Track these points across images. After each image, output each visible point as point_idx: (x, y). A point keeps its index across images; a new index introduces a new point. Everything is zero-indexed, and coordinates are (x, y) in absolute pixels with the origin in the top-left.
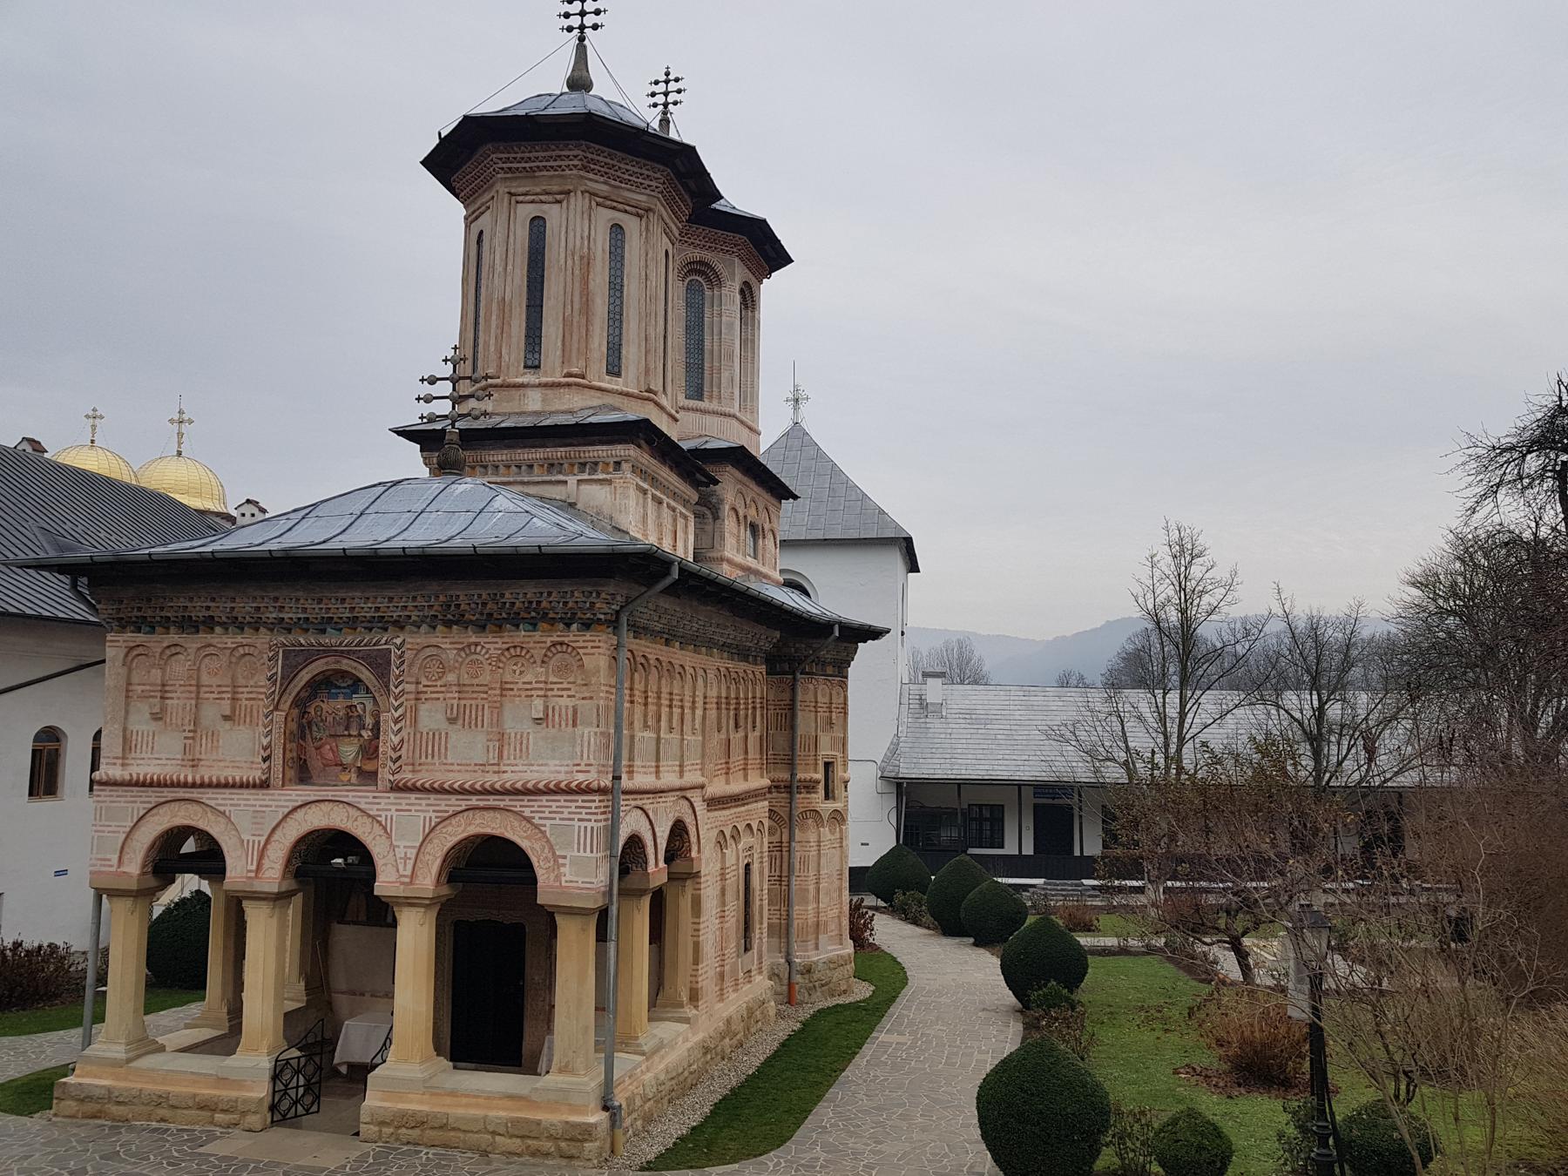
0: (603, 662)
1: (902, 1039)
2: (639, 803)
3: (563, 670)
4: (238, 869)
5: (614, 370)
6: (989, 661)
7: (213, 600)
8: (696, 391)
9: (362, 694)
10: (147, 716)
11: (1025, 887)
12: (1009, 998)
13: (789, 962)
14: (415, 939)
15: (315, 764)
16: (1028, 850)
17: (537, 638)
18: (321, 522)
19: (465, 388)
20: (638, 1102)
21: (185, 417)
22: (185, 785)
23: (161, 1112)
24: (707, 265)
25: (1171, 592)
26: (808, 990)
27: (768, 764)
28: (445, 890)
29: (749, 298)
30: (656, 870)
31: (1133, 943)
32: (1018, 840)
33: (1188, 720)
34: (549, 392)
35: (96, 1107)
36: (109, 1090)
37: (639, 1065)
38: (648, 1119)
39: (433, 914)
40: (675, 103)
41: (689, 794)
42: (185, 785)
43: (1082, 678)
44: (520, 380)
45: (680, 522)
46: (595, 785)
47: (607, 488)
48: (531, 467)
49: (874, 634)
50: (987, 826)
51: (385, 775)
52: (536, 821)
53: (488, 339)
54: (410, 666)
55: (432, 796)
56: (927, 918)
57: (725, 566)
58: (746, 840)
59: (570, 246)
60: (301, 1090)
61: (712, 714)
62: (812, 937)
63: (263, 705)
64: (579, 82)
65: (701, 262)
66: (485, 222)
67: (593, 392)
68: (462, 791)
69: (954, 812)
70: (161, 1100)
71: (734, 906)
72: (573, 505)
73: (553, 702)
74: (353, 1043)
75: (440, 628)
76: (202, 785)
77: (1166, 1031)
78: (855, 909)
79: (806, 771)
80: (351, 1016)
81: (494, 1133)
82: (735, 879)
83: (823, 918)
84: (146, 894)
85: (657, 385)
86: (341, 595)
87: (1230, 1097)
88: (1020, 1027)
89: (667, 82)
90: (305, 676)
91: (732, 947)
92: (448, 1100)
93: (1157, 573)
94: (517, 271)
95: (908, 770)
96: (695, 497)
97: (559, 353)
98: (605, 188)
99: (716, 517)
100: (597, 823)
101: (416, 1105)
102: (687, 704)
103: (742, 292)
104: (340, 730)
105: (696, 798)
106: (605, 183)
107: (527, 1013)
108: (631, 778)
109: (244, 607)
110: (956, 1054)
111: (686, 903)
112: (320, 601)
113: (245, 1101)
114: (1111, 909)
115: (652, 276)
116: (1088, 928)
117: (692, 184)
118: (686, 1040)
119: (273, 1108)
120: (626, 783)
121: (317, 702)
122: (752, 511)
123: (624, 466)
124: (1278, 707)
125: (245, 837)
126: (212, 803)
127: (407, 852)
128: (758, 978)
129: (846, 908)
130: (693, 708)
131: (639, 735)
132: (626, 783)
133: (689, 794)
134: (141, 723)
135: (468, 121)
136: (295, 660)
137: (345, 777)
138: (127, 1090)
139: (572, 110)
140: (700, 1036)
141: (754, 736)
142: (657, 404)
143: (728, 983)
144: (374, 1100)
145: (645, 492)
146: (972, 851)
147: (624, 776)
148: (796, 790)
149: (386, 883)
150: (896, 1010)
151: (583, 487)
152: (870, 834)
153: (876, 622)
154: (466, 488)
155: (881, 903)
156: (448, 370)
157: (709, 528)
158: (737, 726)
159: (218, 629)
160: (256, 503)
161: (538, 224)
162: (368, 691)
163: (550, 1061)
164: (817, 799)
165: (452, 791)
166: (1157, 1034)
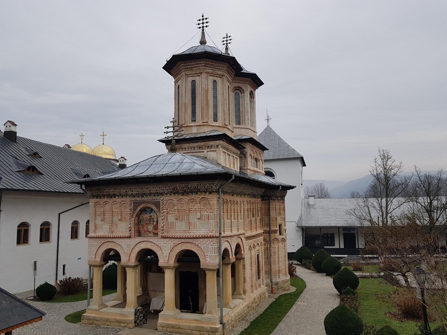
0: (215, 202)
1: (304, 304)
2: (227, 240)
3: (205, 205)
4: (124, 259)
5: (215, 120)
6: (329, 188)
7: (115, 189)
8: (238, 123)
9: (153, 213)
10: (100, 220)
11: (342, 258)
12: (336, 292)
13: (271, 281)
14: (169, 277)
15: (142, 231)
16: (342, 246)
17: (198, 197)
18: (141, 167)
19: (176, 128)
20: (230, 322)
21: (105, 134)
22: (110, 238)
23: (108, 323)
24: (240, 87)
25: (382, 170)
26: (277, 289)
27: (262, 226)
28: (177, 264)
29: (252, 95)
30: (232, 257)
31: (374, 274)
32: (339, 244)
33: (389, 207)
34: (198, 127)
35: (92, 322)
36: (95, 317)
37: (230, 311)
38: (233, 326)
39: (174, 271)
40: (229, 43)
41: (240, 236)
42: (110, 238)
43: (358, 193)
44: (190, 125)
45: (235, 159)
46: (214, 236)
47: (215, 153)
49: (292, 188)
50: (329, 240)
51: (160, 234)
52: (199, 246)
53: (182, 114)
54: (165, 205)
55: (172, 239)
56: (312, 268)
57: (248, 171)
58: (257, 248)
59: (202, 87)
60: (142, 318)
61: (246, 213)
62: (278, 274)
63: (128, 217)
64: (203, 42)
65: (238, 87)
66: (180, 83)
67: (210, 127)
68: (180, 238)
69: (319, 236)
70: (107, 320)
71: (255, 267)
72: (206, 158)
73: (203, 213)
74: (154, 305)
75: (172, 195)
76: (114, 238)
77: (383, 301)
78: (290, 266)
79: (274, 227)
80: (154, 297)
81: (192, 330)
82: (254, 259)
83: (280, 269)
84: (102, 266)
85: (227, 123)
87: (402, 321)
88: (339, 300)
89: (227, 37)
90: (139, 208)
91: (255, 278)
92: (180, 321)
93: (377, 164)
94: (189, 96)
95: (304, 224)
96: (239, 152)
97: (201, 117)
98: (211, 71)
99: (245, 157)
100: (216, 246)
101: (172, 322)
102: (239, 212)
103: (250, 94)
104: (148, 222)
105: (242, 237)
107: (200, 296)
108: (224, 233)
109: (123, 191)
110: (320, 308)
111: (241, 266)
112: (142, 189)
113: (128, 320)
114: (369, 264)
115: (225, 94)
116: (360, 270)
117: (235, 67)
118: (243, 304)
119: (135, 322)
120: (223, 234)
121: (142, 215)
122: (256, 155)
123: (219, 146)
124: (417, 202)
125: (126, 251)
126: (117, 242)
127: (167, 255)
128: (262, 286)
129: (287, 266)
130: (241, 212)
131: (226, 221)
132: (223, 234)
133: (240, 236)
134: (99, 222)
135: (174, 56)
136: (136, 204)
137: (150, 235)
138: (99, 317)
139: (201, 51)
140: (246, 303)
141: (258, 219)
142: (228, 128)
143: (254, 288)
144: (161, 320)
145: (225, 153)
146: (325, 247)
147: (222, 233)
148: (271, 233)
149: (161, 263)
150: (303, 295)
151: (208, 153)
152: (294, 243)
153: (293, 185)
154: (178, 156)
155: (299, 263)
156: (171, 125)
157: (243, 161)
158: (253, 216)
159: (117, 197)
160: (123, 158)
161: (193, 82)
162: (155, 212)
163: (206, 310)
164: (277, 235)
165: (177, 238)
166: (380, 302)
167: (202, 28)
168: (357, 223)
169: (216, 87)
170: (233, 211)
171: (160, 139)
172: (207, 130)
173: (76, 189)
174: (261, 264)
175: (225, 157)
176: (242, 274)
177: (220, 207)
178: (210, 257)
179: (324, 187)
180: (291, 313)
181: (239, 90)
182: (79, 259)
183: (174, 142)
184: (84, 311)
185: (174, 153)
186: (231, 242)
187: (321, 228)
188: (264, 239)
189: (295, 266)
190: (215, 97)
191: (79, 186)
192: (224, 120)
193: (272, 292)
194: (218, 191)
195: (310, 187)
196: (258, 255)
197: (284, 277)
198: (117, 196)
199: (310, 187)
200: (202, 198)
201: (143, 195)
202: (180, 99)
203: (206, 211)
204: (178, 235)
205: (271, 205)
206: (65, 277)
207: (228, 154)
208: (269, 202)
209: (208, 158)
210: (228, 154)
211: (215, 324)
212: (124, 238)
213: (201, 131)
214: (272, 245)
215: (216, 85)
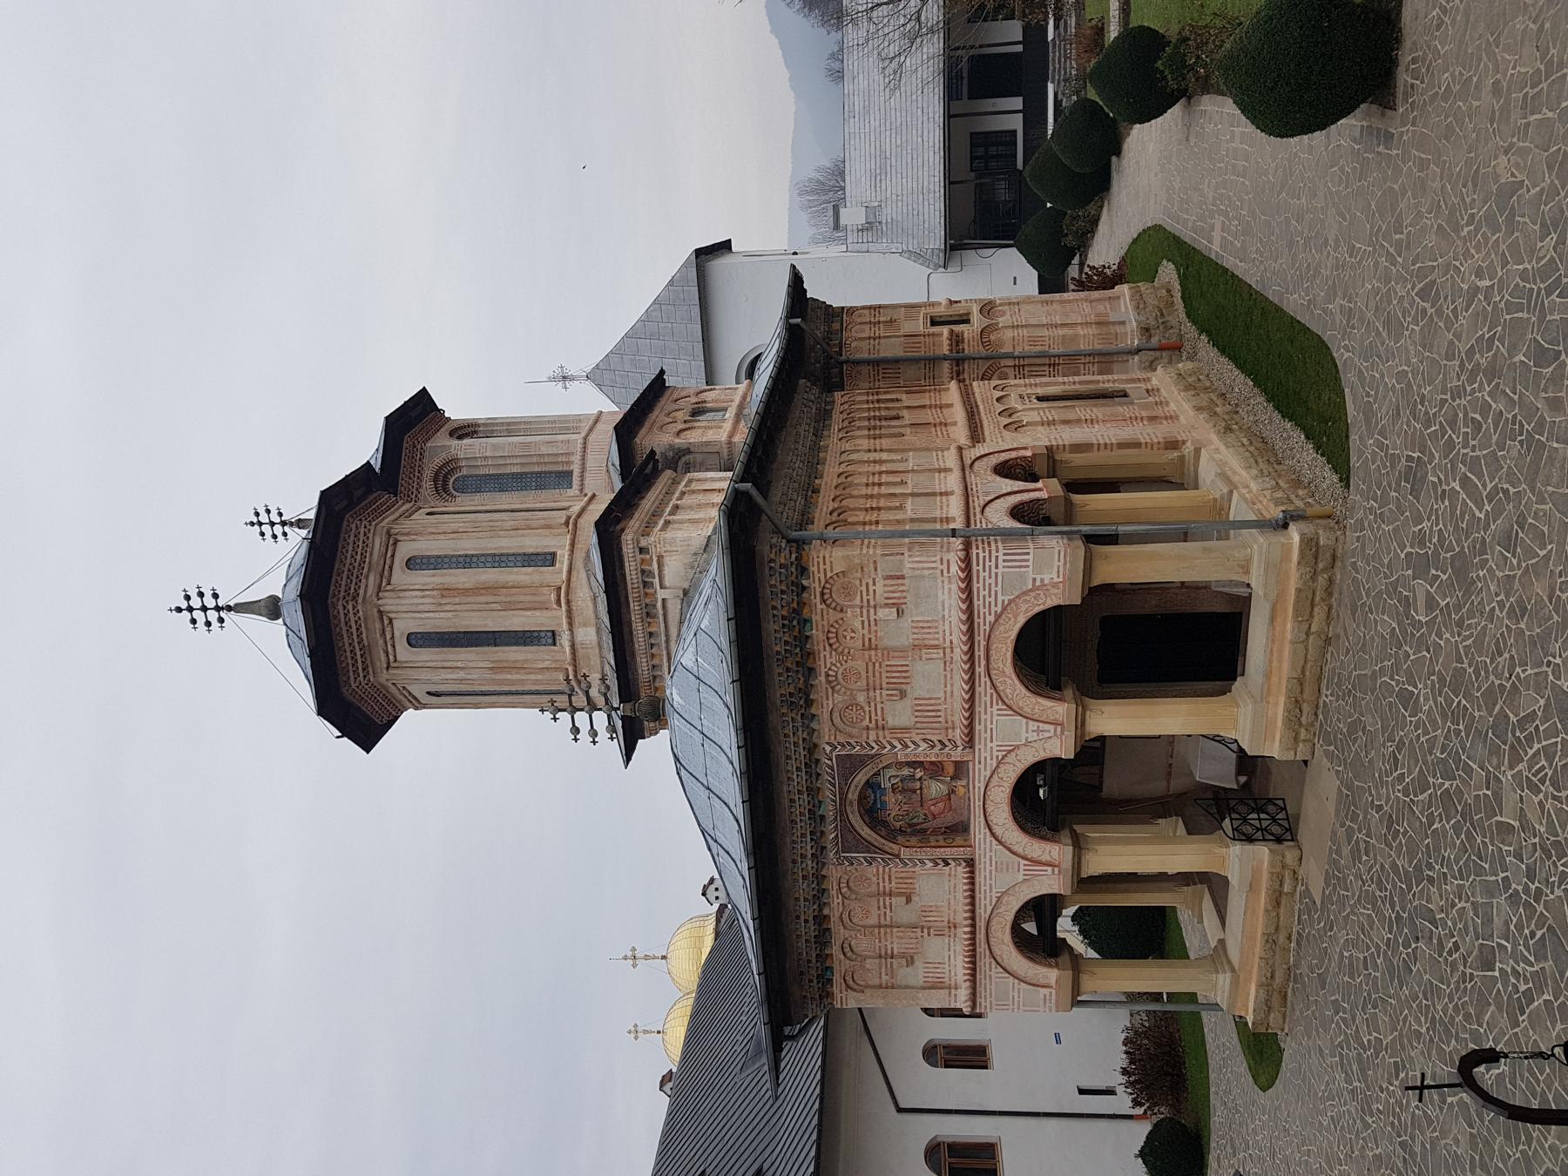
2: (978, 510)
3: (848, 591)
4: (1051, 883)
5: (549, 559)
6: (818, 161)
7: (798, 917)
8: (564, 478)
11: (1057, 103)
12: (1175, 112)
13: (1138, 351)
14: (1116, 719)
15: (949, 819)
16: (1017, 103)
17: (818, 618)
18: (719, 824)
19: (579, 699)
20: (1279, 494)
21: (630, 954)
22: (973, 933)
23: (1282, 939)
24: (437, 474)
27: (936, 385)
28: (1069, 693)
29: (466, 430)
30: (1045, 489)
32: (1007, 114)
34: (577, 620)
35: (1276, 994)
36: (1260, 985)
37: (1242, 495)
38: (1297, 483)
40: (280, 514)
42: (973, 933)
44: (568, 649)
45: (694, 486)
46: (962, 554)
47: (666, 559)
48: (651, 634)
49: (796, 281)
50: (993, 150)
51: (957, 755)
52: (999, 609)
53: (531, 681)
54: (852, 736)
56: (1091, 209)
59: (432, 608)
61: (885, 443)
62: (1112, 329)
63: (895, 869)
64: (272, 608)
65: (435, 480)
66: (418, 691)
68: (972, 682)
70: (1271, 941)
71: (1081, 410)
72: (686, 592)
73: (880, 599)
74: (1218, 772)
75: (813, 711)
76: (973, 918)
78: (1082, 286)
80: (1191, 774)
81: (1308, 634)
82: (1053, 411)
84: (1076, 961)
85: (561, 517)
86: (786, 802)
88: (1206, 97)
89: (260, 524)
90: (866, 832)
91: (1122, 410)
92: (1275, 679)
94: (463, 656)
95: (935, 237)
96: (668, 473)
97: (538, 613)
98: (372, 578)
99: (688, 451)
100: (999, 549)
101: (1279, 709)
102: (877, 468)
103: (460, 438)
105: (970, 455)
106: (367, 577)
107: (1188, 609)
108: (954, 519)
109: (803, 889)
111: (1078, 459)
113: (1272, 865)
115: (454, 526)
116: (1100, 30)
117: (358, 493)
118: (1217, 450)
119: (1279, 840)
120: (958, 524)
122: (680, 415)
123: (643, 543)
125: (1021, 878)
126: (989, 909)
127: (1031, 730)
128: (1154, 381)
130: (881, 462)
131: (909, 514)
132: (958, 524)
136: (851, 842)
137: (961, 791)
140: (1214, 437)
141: (907, 400)
142: (579, 515)
143: (1159, 412)
144: (1274, 749)
145: (667, 523)
147: (952, 526)
148: (959, 354)
149: (1062, 747)
150: (1187, 235)
151: (667, 584)
152: (1005, 275)
154: (676, 694)
157: (699, 458)
158: (897, 418)
159: (826, 912)
160: (705, 888)
161: (414, 640)
162: (877, 774)
164: (968, 331)
167: (223, 614)
168: (933, 47)
169: (429, 557)
170: (876, 490)
171: (619, 758)
172: (586, 589)
173: (804, 1056)
174: (1073, 387)
175: (681, 522)
176: (1108, 452)
177: (857, 536)
178: (1039, 569)
179: (810, 180)
180: (1250, 274)
181: (445, 476)
182: (1058, 1039)
183: (629, 706)
184: (1240, 1023)
185: (667, 706)
186: (988, 493)
187: (951, 182)
188: (984, 377)
189: (1087, 269)
190: (467, 561)
191: (787, 1045)
192: (548, 527)
193: (1178, 348)
194: (796, 541)
195: (812, 231)
196: (1040, 399)
197: (1123, 302)
198: (821, 910)
199: (812, 231)
200: (824, 601)
201: (817, 818)
202: (477, 688)
203: (871, 588)
204: (959, 686)
205: (858, 356)
206: (1120, 1090)
207: (672, 513)
208: (847, 362)
209: (686, 585)
210: (672, 513)
211: (1287, 549)
212: (973, 884)
213: (590, 612)
214: (1007, 349)
215: (423, 557)
